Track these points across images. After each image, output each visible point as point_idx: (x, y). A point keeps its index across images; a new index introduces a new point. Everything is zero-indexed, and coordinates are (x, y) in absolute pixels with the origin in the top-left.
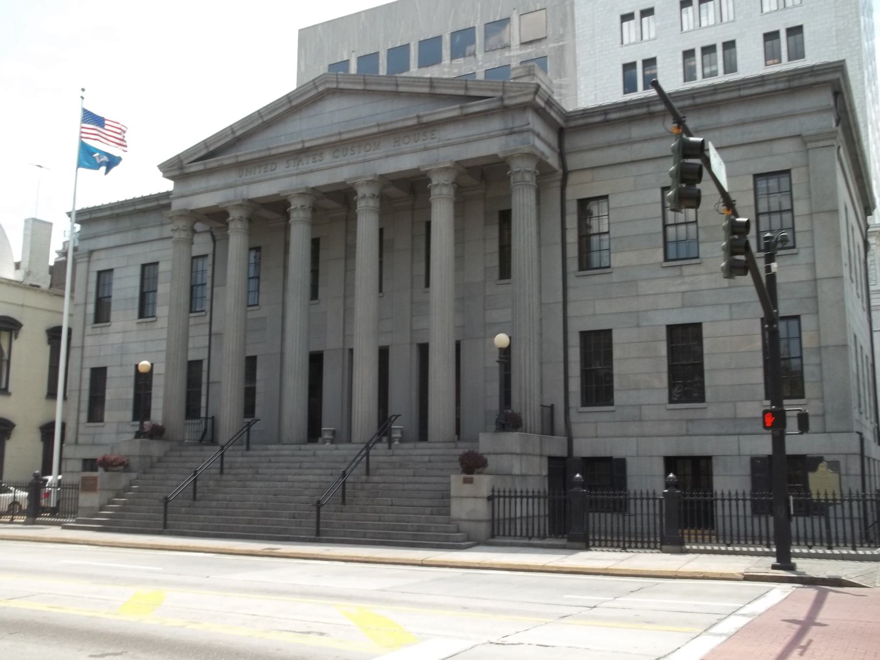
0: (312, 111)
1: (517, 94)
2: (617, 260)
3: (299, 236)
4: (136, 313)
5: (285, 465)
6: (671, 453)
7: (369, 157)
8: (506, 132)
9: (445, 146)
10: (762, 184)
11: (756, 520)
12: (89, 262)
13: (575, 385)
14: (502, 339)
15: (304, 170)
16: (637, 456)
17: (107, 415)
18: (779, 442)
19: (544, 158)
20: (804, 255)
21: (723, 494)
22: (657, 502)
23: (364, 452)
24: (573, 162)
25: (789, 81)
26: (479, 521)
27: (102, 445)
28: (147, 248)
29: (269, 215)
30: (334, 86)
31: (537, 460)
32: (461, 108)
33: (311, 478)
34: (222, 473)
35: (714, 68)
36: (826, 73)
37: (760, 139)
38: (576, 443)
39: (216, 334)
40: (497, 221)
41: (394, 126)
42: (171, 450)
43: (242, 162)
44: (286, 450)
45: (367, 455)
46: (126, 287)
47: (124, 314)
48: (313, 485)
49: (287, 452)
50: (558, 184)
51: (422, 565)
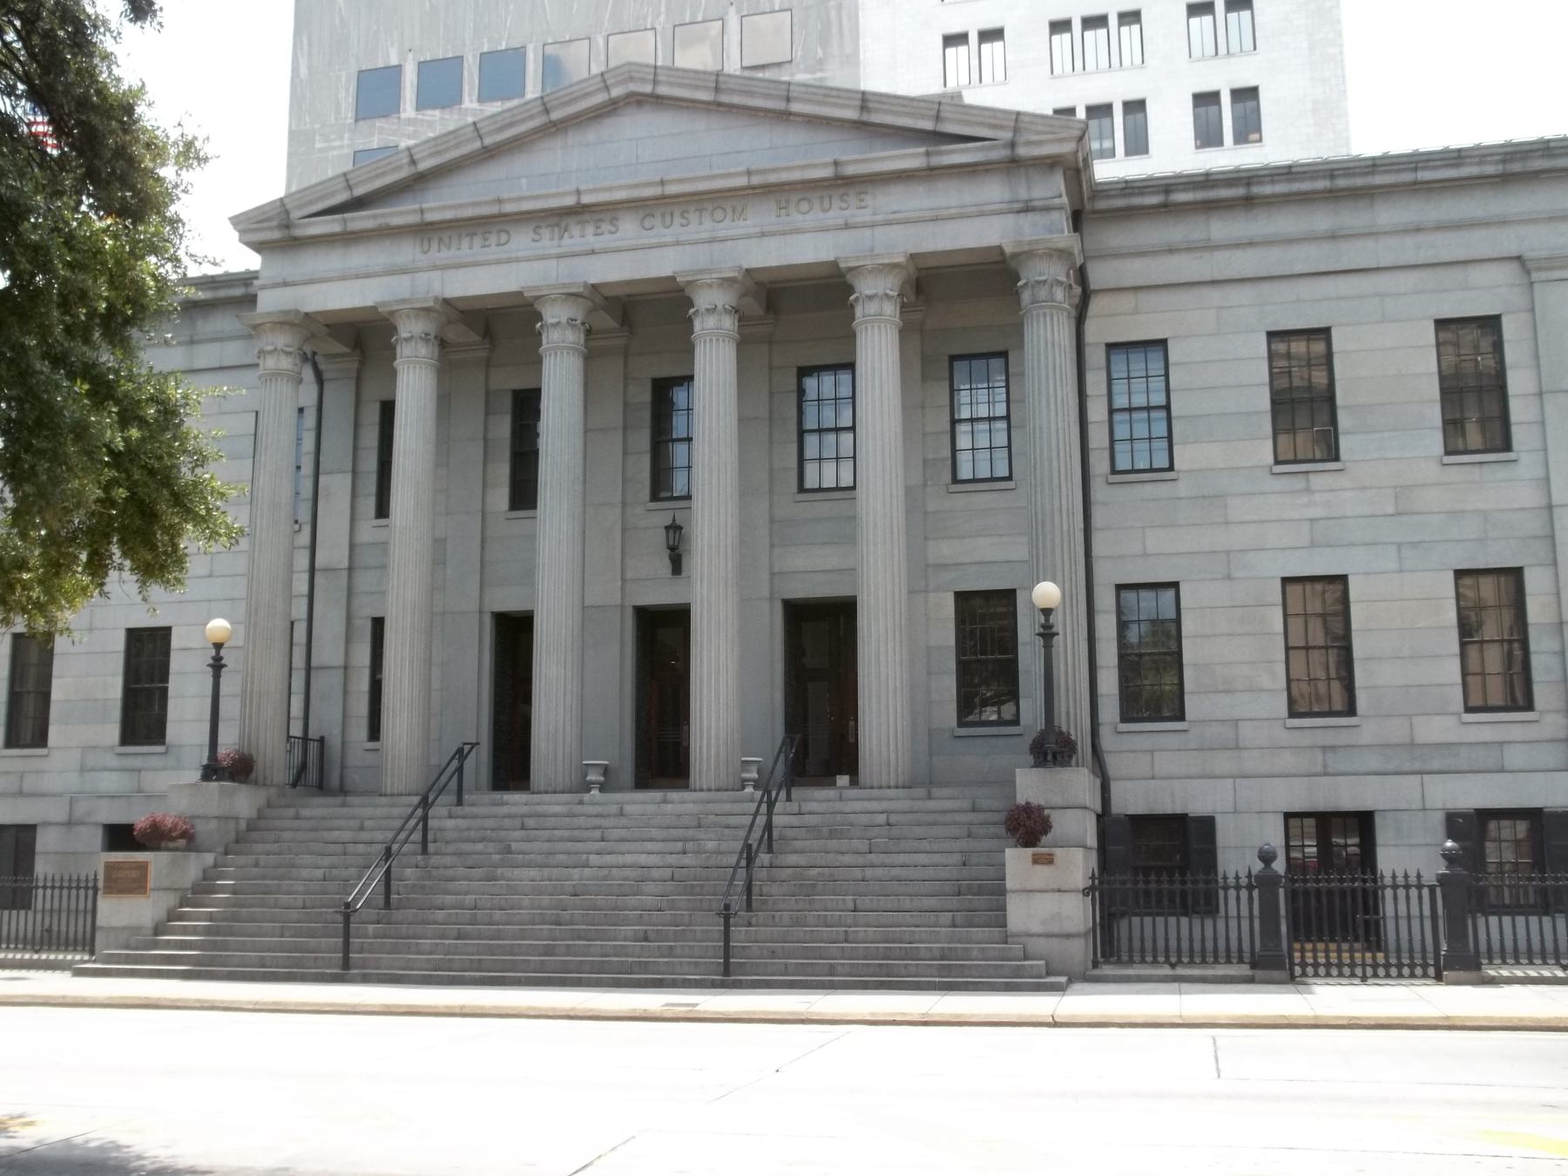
0: (591, 134)
5: (566, 833)
7: (721, 234)
8: (1016, 206)
13: (1109, 683)
15: (577, 249)
21: (1394, 877)
22: (1425, 892)
23: (419, 812)
25: (1504, 162)
26: (1068, 936)
27: (43, 795)
30: (648, 89)
32: (928, 154)
33: (643, 859)
34: (425, 851)
35: (1107, 144)
37: (1449, 259)
38: (1116, 789)
39: (325, 570)
41: (785, 177)
42: (269, 805)
43: (431, 224)
45: (425, 819)
48: (656, 873)
49: (558, 809)
51: (926, 1024)
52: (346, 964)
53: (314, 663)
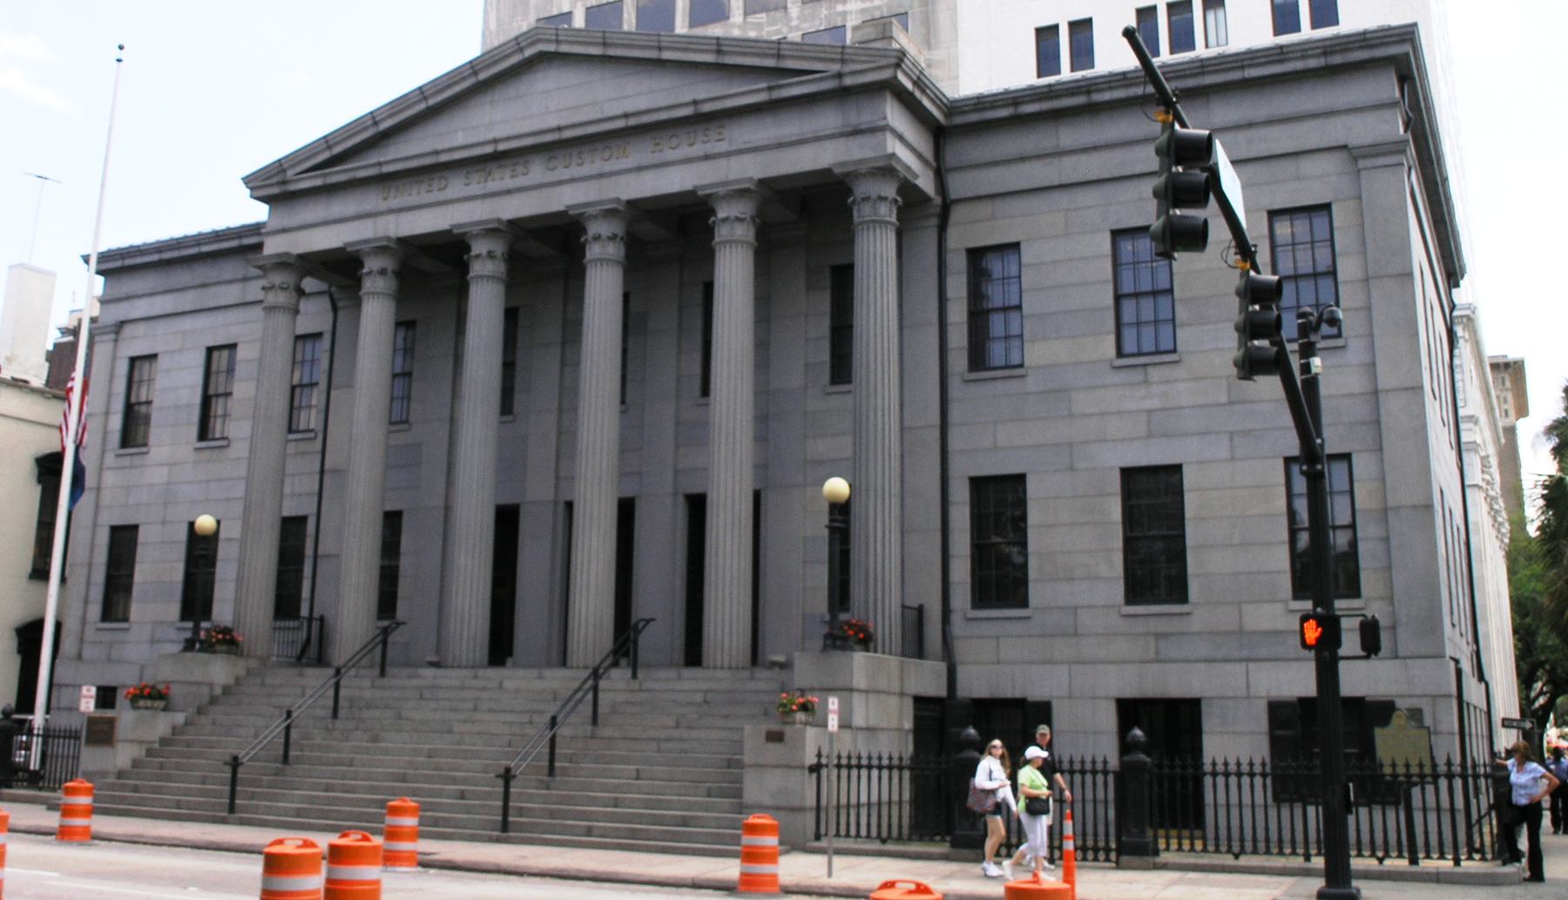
1: (865, 66)
2: (1035, 354)
3: (485, 304)
4: (194, 431)
6: (1130, 692)
9: (740, 152)
10: (1127, 246)
11: (1273, 813)
12: (116, 341)
13: (961, 570)
14: (837, 486)
16: (1070, 697)
17: (136, 610)
18: (1327, 673)
19: (910, 177)
20: (1355, 352)
23: (590, 683)
24: (959, 185)
28: (219, 318)
29: (432, 269)
31: (894, 701)
36: (1386, 44)
37: (1279, 152)
38: (963, 673)
40: (827, 282)
44: (449, 677)
45: (595, 689)
46: (176, 387)
47: (172, 436)
50: (934, 221)
52: (232, 808)
53: (320, 552)
